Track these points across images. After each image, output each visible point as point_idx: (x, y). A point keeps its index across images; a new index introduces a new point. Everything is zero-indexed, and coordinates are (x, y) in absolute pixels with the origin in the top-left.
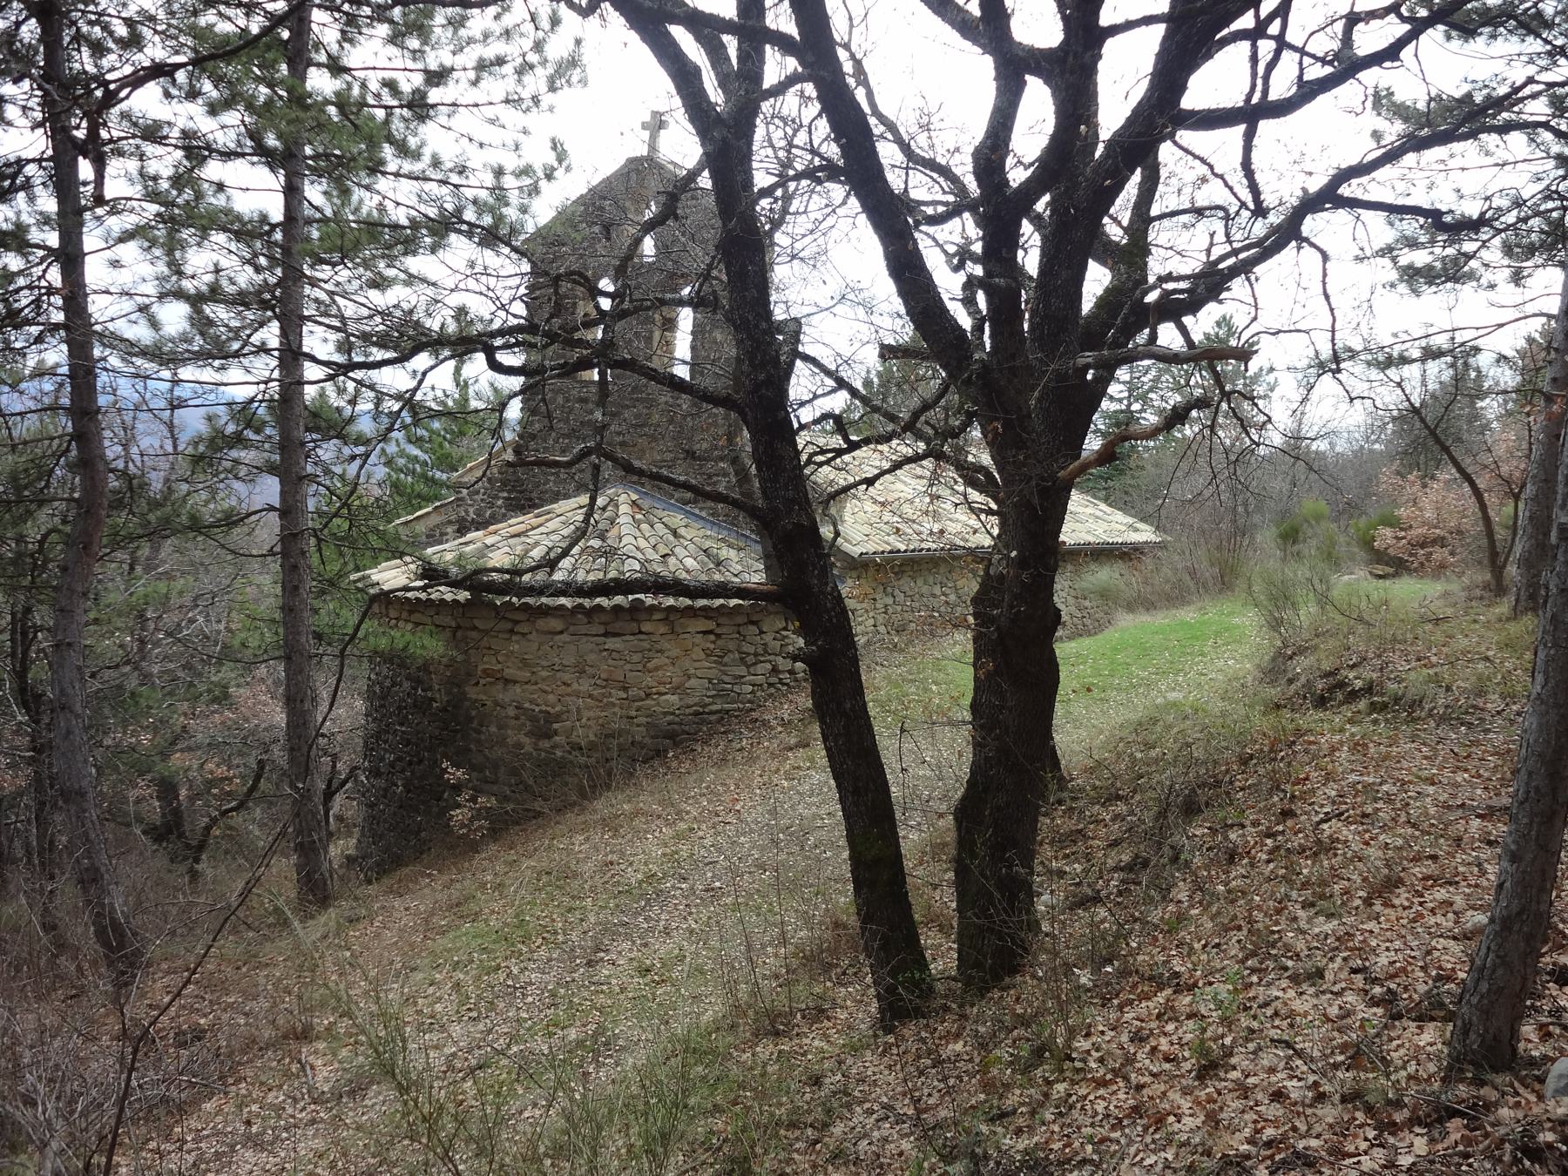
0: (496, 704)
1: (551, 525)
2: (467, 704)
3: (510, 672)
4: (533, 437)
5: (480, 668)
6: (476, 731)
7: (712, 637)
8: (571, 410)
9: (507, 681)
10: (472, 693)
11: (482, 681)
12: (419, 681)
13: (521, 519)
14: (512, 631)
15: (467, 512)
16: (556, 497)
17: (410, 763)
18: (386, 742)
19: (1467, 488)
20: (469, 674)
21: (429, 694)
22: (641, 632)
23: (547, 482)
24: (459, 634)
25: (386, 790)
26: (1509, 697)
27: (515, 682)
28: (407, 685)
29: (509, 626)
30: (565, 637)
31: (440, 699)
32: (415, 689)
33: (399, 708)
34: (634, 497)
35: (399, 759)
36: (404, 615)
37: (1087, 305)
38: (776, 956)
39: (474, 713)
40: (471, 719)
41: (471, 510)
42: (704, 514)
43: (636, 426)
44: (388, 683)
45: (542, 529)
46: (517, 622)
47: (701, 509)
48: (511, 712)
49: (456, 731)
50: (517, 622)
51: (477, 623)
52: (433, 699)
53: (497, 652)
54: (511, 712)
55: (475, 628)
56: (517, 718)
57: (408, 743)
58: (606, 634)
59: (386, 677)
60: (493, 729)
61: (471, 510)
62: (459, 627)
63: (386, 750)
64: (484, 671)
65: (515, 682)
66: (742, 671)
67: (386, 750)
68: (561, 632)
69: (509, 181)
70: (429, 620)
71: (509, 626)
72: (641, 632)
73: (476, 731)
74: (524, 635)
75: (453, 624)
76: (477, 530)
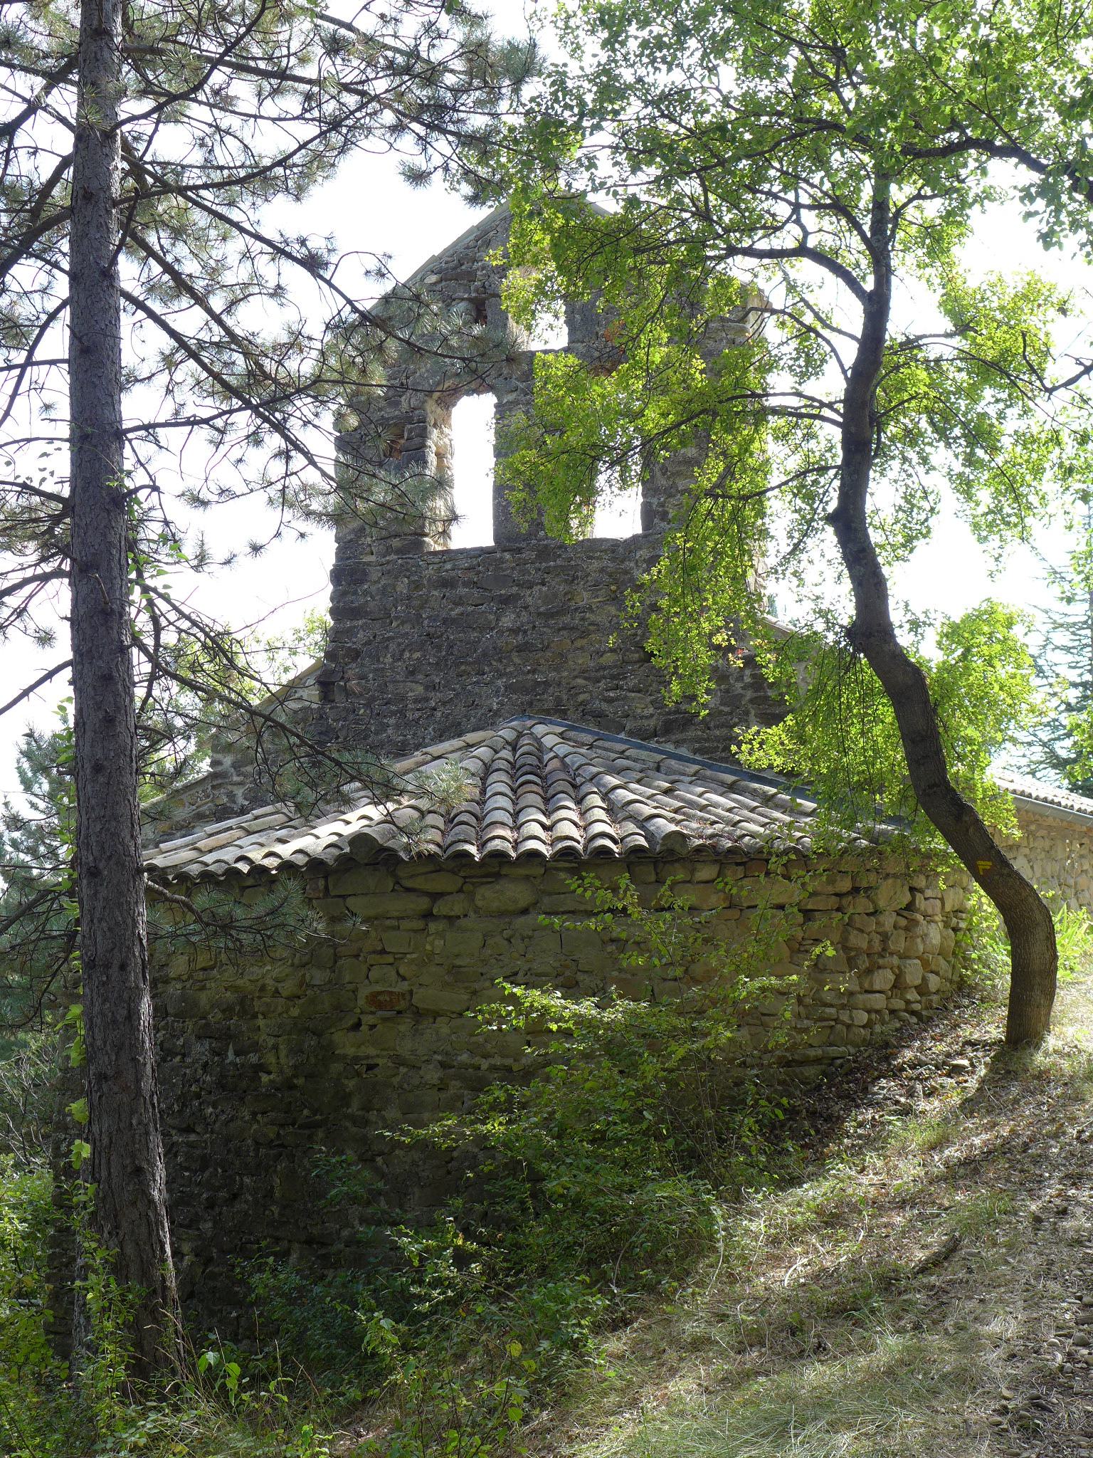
0: (399, 1061)
2: (336, 1067)
3: (423, 998)
4: (355, 655)
5: (364, 992)
6: (355, 1121)
8: (425, 602)
9: (419, 1014)
10: (347, 1044)
11: (368, 1019)
12: (227, 1036)
14: (428, 916)
17: (211, 1204)
21: (253, 1058)
23: (384, 727)
26: (94, 1349)
27: (436, 1015)
28: (201, 1050)
29: (424, 903)
31: (279, 1062)
32: (220, 1053)
38: (470, 1435)
39: (351, 1084)
40: (345, 1099)
41: (239, 792)
42: (683, 751)
43: (549, 615)
46: (436, 896)
47: (678, 743)
48: (432, 1075)
49: (316, 1125)
50: (436, 896)
54: (432, 1075)
57: (205, 1162)
61: (239, 792)
64: (374, 999)
65: (436, 1015)
68: (525, 911)
71: (424, 903)
73: (355, 1121)
74: (451, 919)
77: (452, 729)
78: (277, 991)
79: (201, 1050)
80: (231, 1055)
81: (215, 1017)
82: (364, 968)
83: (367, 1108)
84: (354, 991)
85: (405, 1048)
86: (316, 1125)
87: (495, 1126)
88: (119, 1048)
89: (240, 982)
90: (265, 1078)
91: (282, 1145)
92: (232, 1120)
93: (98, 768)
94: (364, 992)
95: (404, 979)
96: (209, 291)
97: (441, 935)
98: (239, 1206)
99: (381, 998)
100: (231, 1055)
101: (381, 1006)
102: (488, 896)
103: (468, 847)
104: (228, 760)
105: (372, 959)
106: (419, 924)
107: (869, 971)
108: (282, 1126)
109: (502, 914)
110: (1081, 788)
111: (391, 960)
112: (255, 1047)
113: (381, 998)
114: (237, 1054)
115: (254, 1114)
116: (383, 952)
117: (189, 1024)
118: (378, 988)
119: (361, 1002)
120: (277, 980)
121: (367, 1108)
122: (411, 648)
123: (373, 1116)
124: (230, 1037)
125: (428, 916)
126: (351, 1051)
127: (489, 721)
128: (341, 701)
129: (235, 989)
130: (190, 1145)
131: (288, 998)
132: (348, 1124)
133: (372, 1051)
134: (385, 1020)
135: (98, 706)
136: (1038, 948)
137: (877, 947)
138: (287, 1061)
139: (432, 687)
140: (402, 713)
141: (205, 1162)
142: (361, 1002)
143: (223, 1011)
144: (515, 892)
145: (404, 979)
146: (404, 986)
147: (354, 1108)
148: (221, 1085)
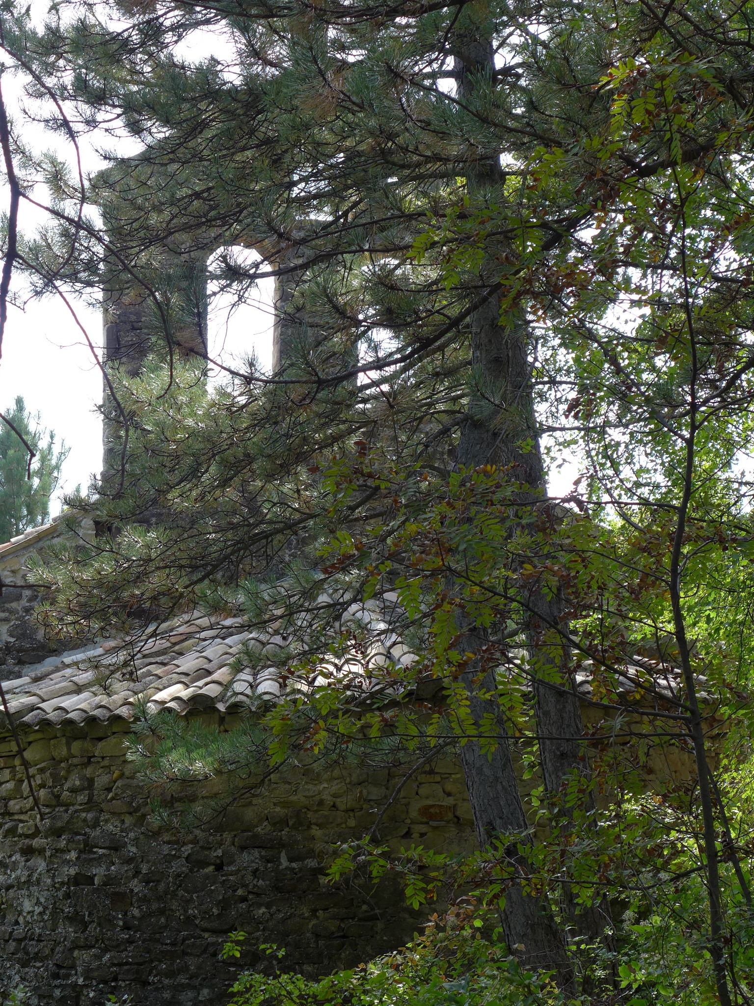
21: (311, 863)
32: (273, 860)
78: (334, 806)
80: (284, 863)
82: (415, 786)
84: (407, 805)
89: (294, 798)
90: (323, 880)
91: (344, 937)
92: (290, 917)
95: (449, 794)
96: (506, 589)
99: (432, 810)
100: (284, 863)
105: (422, 778)
108: (342, 920)
110: (640, 918)
111: (438, 779)
113: (432, 810)
114: (291, 860)
115: (314, 911)
116: (432, 772)
117: (227, 836)
118: (429, 802)
119: (414, 813)
120: (335, 796)
124: (283, 846)
129: (285, 804)
131: (347, 811)
132: (407, 916)
134: (435, 828)
142: (414, 813)
143: (274, 824)
145: (449, 794)
146: (450, 801)
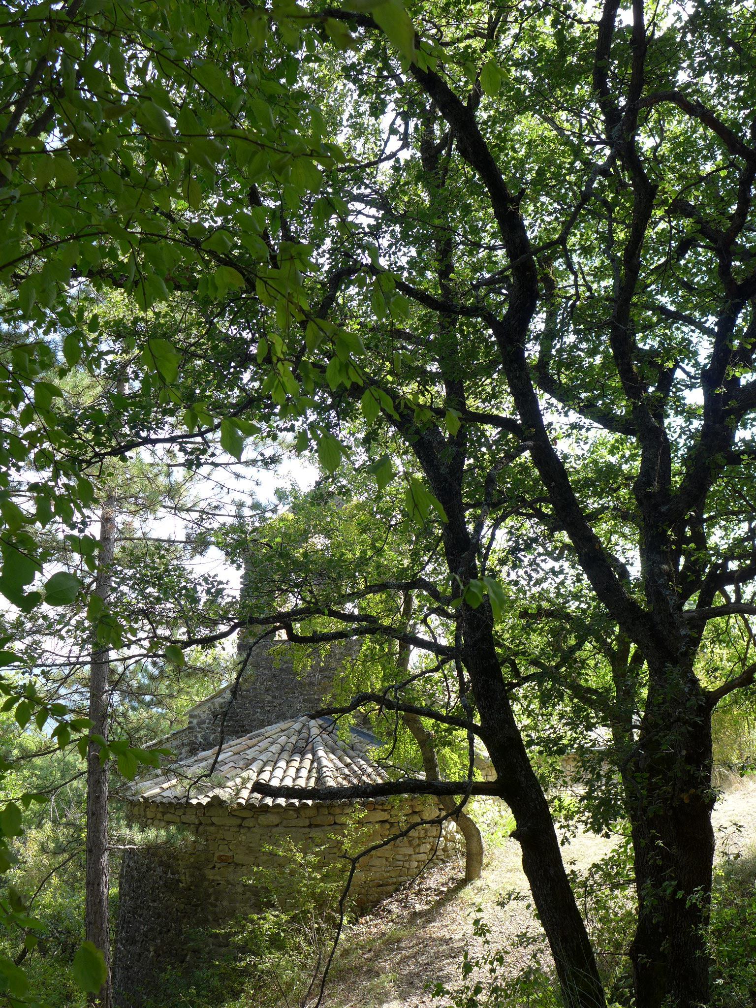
0: (228, 883)
1: (264, 744)
2: (206, 883)
3: (239, 858)
5: (217, 855)
6: (211, 904)
7: (387, 826)
9: (236, 865)
10: (210, 874)
11: (218, 865)
12: (168, 866)
13: (239, 741)
15: (196, 737)
16: (262, 725)
18: (141, 916)
19: (373, 852)
20: (208, 861)
21: (177, 877)
22: (335, 823)
23: (256, 713)
24: (201, 828)
25: (140, 955)
27: (243, 865)
28: (159, 870)
29: (239, 821)
30: (280, 829)
31: (186, 879)
33: (153, 889)
34: (321, 722)
35: (151, 930)
36: (159, 816)
37: (698, 593)
39: (211, 890)
41: (199, 735)
44: (144, 869)
45: (256, 748)
49: (197, 906)
50: (244, 819)
51: (215, 820)
52: (179, 881)
53: (229, 842)
55: (213, 824)
56: (244, 894)
58: (310, 826)
59: (142, 864)
60: (225, 903)
61: (199, 735)
62: (201, 824)
63: (141, 923)
64: (220, 857)
65: (243, 865)
66: (410, 851)
67: (141, 923)
68: (277, 825)
69: (247, 512)
70: (178, 820)
71: (239, 821)
72: (335, 823)
75: (197, 822)
76: (204, 750)
77: (282, 717)
79: (159, 870)
81: (165, 858)
83: (216, 900)
85: (231, 878)
86: (197, 906)
87: (707, 570)
88: (95, 913)
93: (93, 814)
94: (217, 855)
97: (245, 834)
98: (170, 935)
101: (222, 861)
102: (263, 819)
103: (695, 337)
104: (195, 721)
106: (237, 829)
107: (419, 845)
109: (269, 826)
112: (178, 872)
121: (216, 900)
122: (267, 680)
123: (218, 903)
125: (240, 826)
126: (211, 877)
127: (294, 717)
128: (240, 700)
130: (155, 908)
133: (219, 878)
135: (95, 792)
136: (474, 845)
137: (422, 835)
138: (189, 880)
139: (274, 697)
140: (263, 707)
141: (159, 916)
144: (273, 819)
146: (231, 853)
147: (212, 900)
148: (165, 885)
